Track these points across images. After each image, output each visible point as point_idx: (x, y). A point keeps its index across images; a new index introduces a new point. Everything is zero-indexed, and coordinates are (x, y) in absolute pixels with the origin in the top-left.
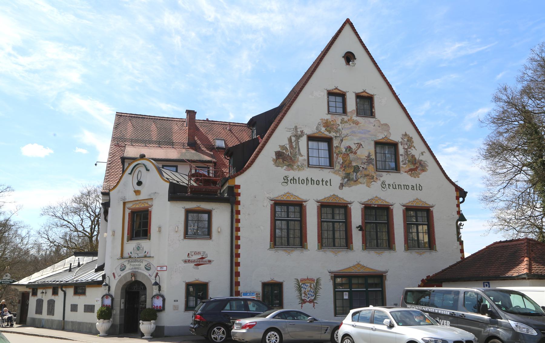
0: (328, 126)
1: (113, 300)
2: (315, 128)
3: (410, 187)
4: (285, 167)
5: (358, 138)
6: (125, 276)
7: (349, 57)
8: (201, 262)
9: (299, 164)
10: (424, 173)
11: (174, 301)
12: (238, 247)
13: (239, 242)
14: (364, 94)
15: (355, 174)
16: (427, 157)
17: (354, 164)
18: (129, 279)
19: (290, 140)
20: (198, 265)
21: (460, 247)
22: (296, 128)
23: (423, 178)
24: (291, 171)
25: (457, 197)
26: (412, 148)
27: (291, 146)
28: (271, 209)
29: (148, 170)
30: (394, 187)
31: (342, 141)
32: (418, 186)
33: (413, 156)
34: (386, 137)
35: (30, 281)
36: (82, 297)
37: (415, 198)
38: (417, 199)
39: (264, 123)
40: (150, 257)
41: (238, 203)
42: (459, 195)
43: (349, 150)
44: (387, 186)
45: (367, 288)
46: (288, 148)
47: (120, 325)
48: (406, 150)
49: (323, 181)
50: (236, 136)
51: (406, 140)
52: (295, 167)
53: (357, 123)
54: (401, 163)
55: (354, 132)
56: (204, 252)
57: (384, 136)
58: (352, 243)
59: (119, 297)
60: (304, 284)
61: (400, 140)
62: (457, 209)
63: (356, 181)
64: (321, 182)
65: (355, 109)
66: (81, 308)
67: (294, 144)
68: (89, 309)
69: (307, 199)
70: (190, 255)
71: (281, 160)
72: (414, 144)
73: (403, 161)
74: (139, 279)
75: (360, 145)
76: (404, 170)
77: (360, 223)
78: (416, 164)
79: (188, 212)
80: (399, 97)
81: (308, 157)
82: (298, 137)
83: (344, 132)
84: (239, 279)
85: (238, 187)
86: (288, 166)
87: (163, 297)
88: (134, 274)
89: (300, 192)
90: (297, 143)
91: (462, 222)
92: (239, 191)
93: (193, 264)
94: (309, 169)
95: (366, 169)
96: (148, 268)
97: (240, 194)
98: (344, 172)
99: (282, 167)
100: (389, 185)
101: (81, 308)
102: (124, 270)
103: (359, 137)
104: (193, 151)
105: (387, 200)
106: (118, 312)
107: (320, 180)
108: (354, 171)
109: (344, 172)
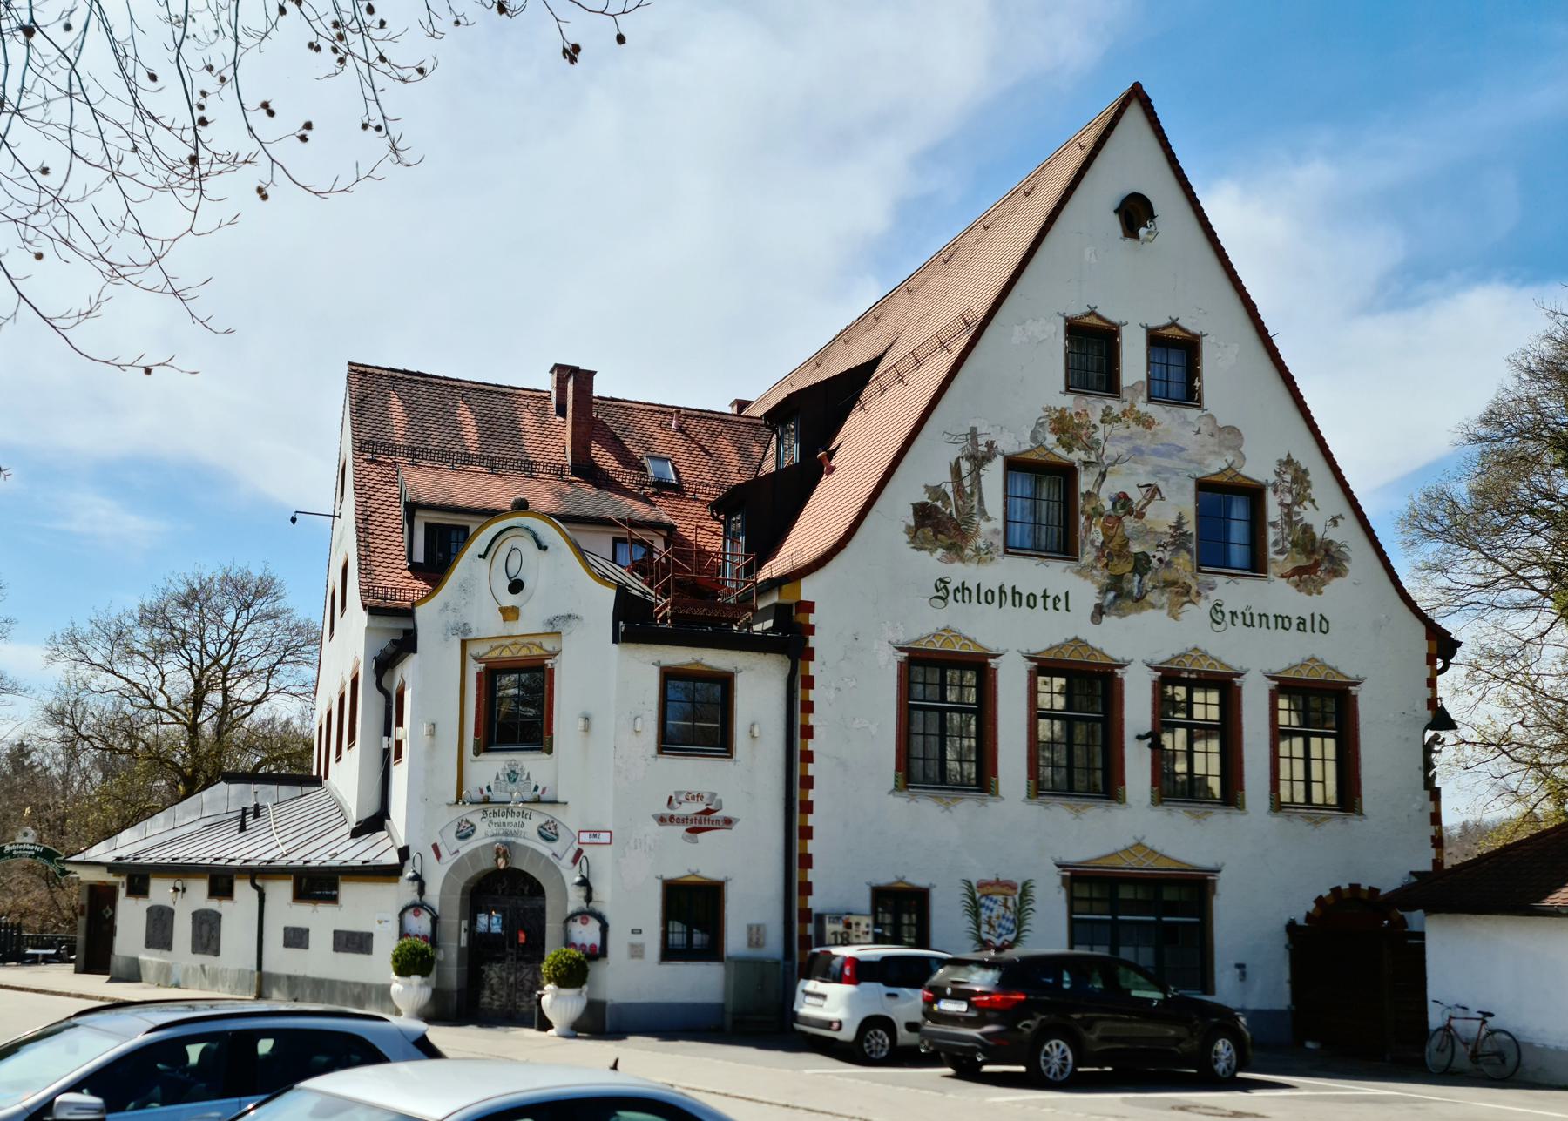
0: (1064, 431)
1: (435, 921)
2: (1028, 434)
3: (1295, 622)
4: (940, 551)
5: (1149, 468)
6: (474, 855)
7: (1135, 213)
8: (705, 821)
9: (980, 542)
10: (1336, 582)
11: (633, 931)
12: (808, 782)
13: (812, 770)
14: (1173, 332)
15: (1137, 578)
16: (1346, 535)
17: (1135, 548)
18: (487, 864)
19: (956, 470)
20: (694, 831)
21: (1431, 807)
22: (974, 433)
23: (1335, 597)
24: (958, 565)
25: (1428, 656)
26: (1306, 503)
27: (959, 490)
28: (899, 676)
29: (542, 547)
30: (1248, 621)
31: (1103, 475)
32: (1317, 618)
33: (1307, 529)
34: (1230, 467)
35: (118, 854)
36: (324, 910)
37: (1308, 656)
38: (1076, 639)
39: (817, 410)
40: (555, 802)
41: (809, 655)
42: (1435, 651)
43: (1123, 507)
44: (1228, 617)
45: (1114, 913)
46: (951, 496)
47: (459, 991)
48: (1288, 510)
49: (1045, 596)
50: (702, 448)
51: (1288, 478)
52: (968, 552)
53: (1147, 422)
54: (1271, 550)
55: (1137, 452)
56: (713, 795)
57: (1224, 466)
58: (1123, 783)
59: (456, 913)
60: (986, 896)
61: (1272, 478)
62: (1428, 693)
63: (1139, 600)
64: (1040, 601)
65: (1144, 378)
66: (321, 940)
67: (967, 482)
68: (353, 942)
69: (1002, 649)
70: (675, 803)
71: (929, 532)
72: (1313, 492)
73: (1276, 543)
74: (522, 864)
75: (1153, 491)
76: (1279, 571)
77: (1146, 727)
78: (1313, 552)
79: (669, 676)
80: (1276, 341)
81: (1006, 521)
82: (979, 461)
83: (1111, 450)
84: (811, 875)
85: (809, 607)
86: (948, 548)
87: (600, 918)
88: (505, 850)
89: (982, 628)
90: (977, 480)
91: (1443, 734)
92: (812, 619)
93: (682, 829)
94: (1008, 559)
95: (1168, 564)
96: (548, 834)
97: (813, 627)
98: (1107, 573)
99: (932, 551)
100: (1233, 614)
101: (321, 940)
102: (467, 836)
103: (1148, 465)
104: (594, 491)
105: (1226, 660)
106: (454, 956)
107: (1039, 594)
108: (1134, 571)
109: (1107, 573)
